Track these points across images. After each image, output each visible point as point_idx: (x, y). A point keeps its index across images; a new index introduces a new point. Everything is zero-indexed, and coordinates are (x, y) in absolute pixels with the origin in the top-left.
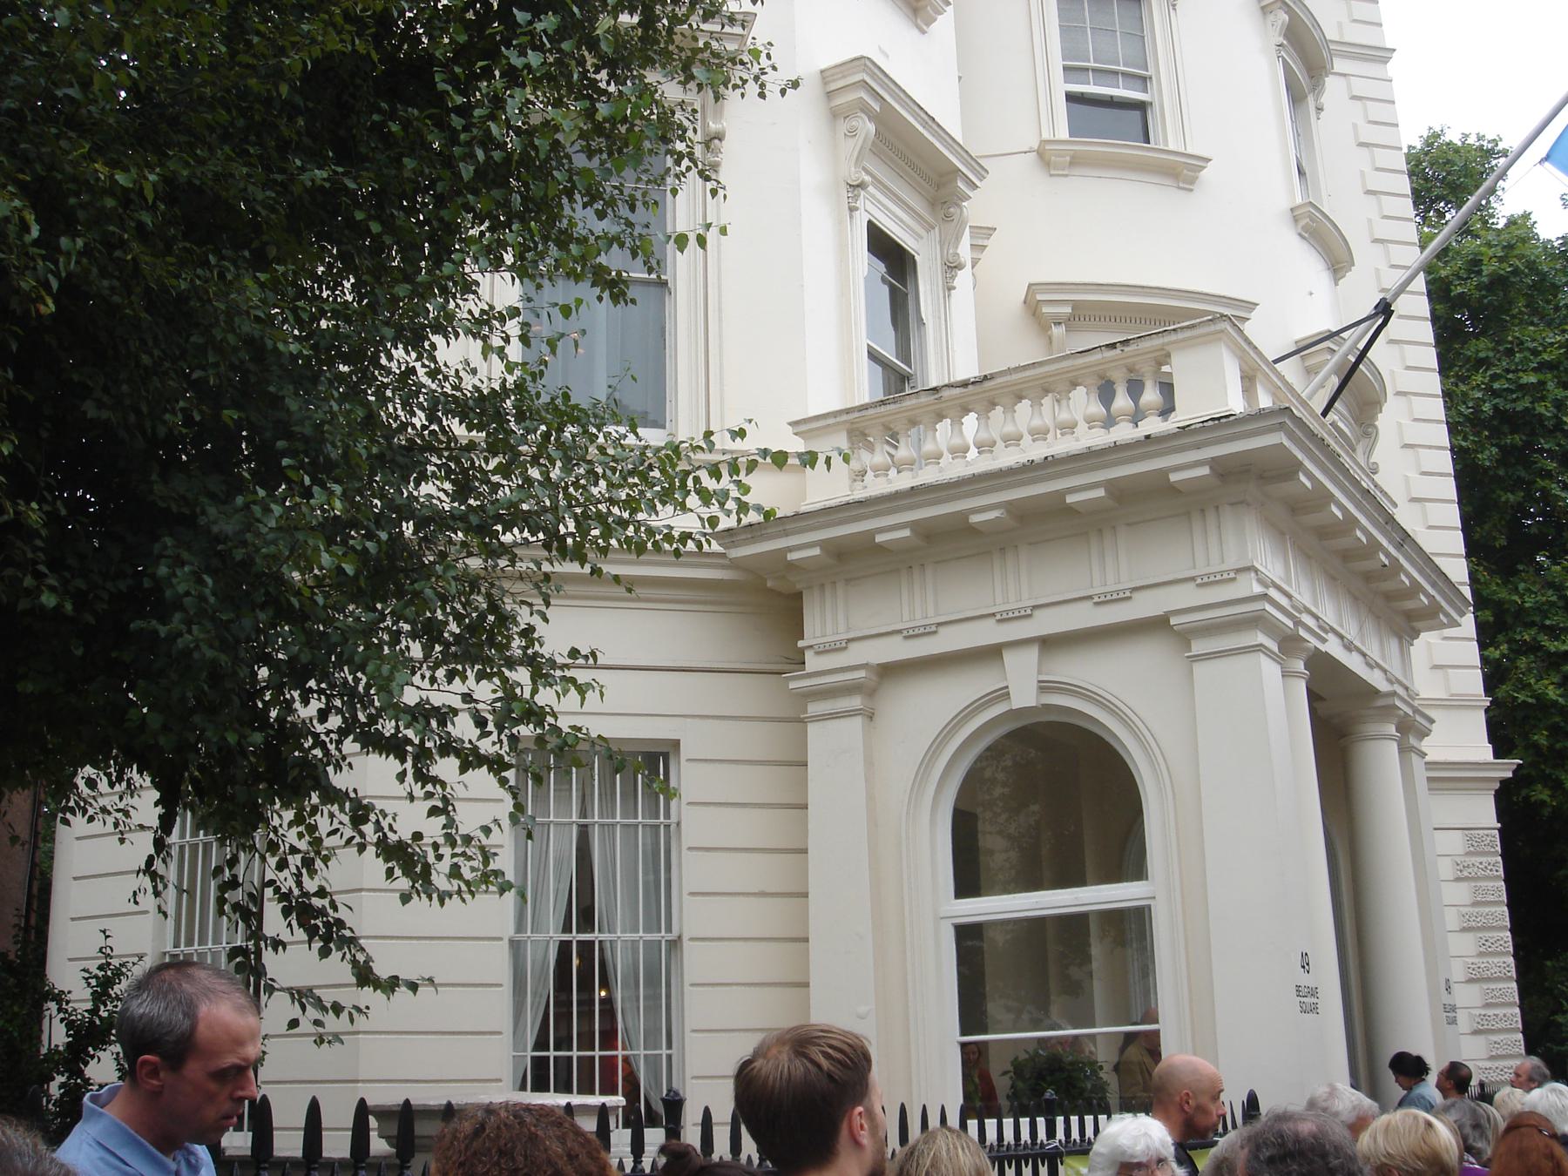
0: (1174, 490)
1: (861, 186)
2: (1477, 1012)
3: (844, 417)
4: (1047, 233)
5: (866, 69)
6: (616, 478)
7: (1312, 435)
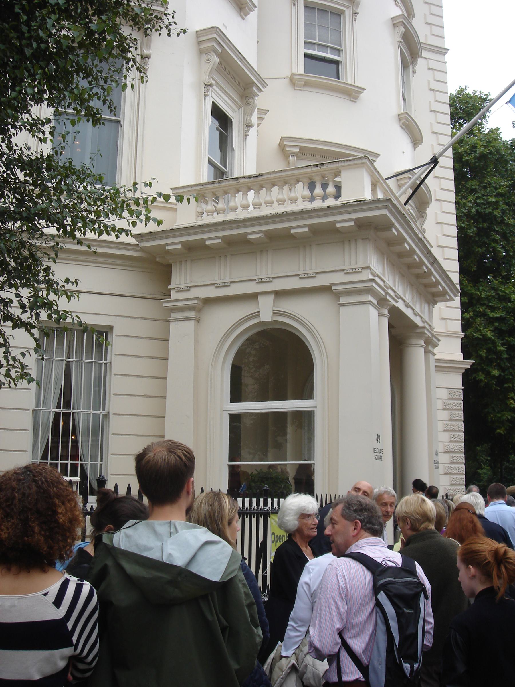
0: (338, 231)
1: (210, 85)
2: (447, 465)
3: (196, 188)
4: (290, 114)
5: (216, 33)
6: (91, 201)
7: (399, 212)
